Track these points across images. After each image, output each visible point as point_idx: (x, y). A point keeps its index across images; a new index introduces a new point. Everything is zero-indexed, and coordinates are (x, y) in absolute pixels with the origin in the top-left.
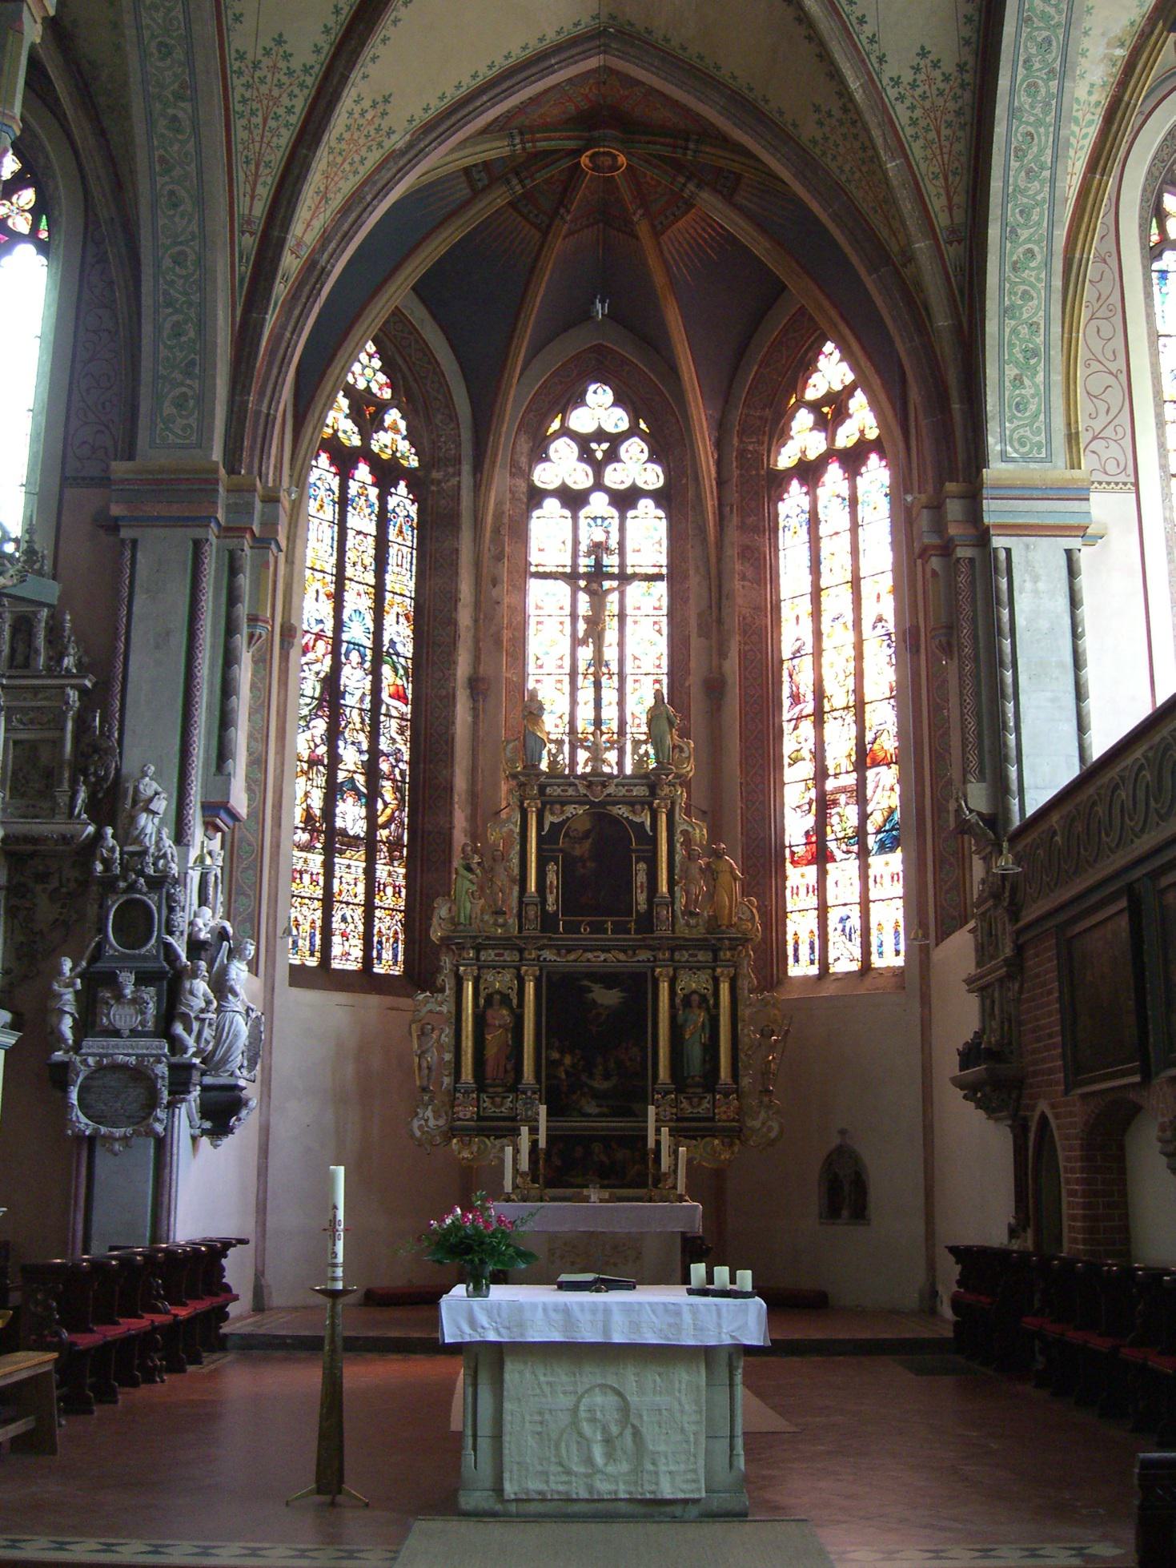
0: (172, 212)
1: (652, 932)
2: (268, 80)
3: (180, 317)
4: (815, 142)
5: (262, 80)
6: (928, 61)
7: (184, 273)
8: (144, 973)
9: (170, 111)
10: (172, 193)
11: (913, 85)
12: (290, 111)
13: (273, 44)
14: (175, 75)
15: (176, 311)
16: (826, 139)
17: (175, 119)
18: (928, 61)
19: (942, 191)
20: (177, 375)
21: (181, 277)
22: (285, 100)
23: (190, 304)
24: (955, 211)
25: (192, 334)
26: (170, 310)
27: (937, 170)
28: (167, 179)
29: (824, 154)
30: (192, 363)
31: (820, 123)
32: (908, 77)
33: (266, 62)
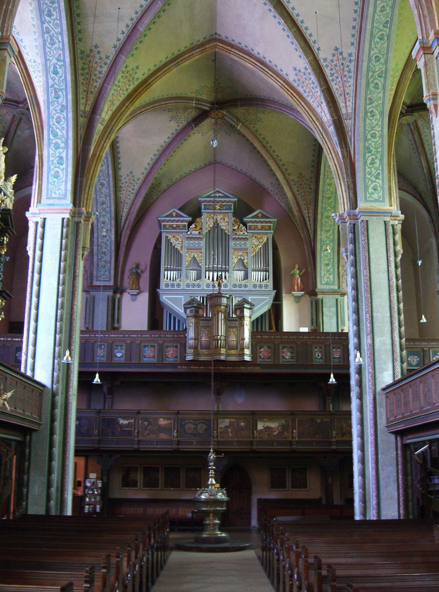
0: (371, 118)
1: (344, 336)
2: (338, 65)
3: (374, 157)
4: (295, 81)
5: (336, 66)
6: (338, 52)
7: (375, 140)
8: (154, 487)
9: (375, 81)
10: (372, 112)
11: (332, 61)
12: (100, 73)
13: (334, 51)
14: (380, 68)
15: (372, 155)
16: (299, 80)
17: (377, 84)
18: (338, 52)
19: (85, 97)
20: (374, 179)
21: (374, 142)
22: (98, 69)
23: (377, 152)
24: (87, 106)
25: (378, 163)
26: (370, 154)
27: (85, 89)
28: (371, 106)
29: (298, 85)
30: (379, 174)
31: (296, 75)
32: (330, 57)
33: (335, 58)
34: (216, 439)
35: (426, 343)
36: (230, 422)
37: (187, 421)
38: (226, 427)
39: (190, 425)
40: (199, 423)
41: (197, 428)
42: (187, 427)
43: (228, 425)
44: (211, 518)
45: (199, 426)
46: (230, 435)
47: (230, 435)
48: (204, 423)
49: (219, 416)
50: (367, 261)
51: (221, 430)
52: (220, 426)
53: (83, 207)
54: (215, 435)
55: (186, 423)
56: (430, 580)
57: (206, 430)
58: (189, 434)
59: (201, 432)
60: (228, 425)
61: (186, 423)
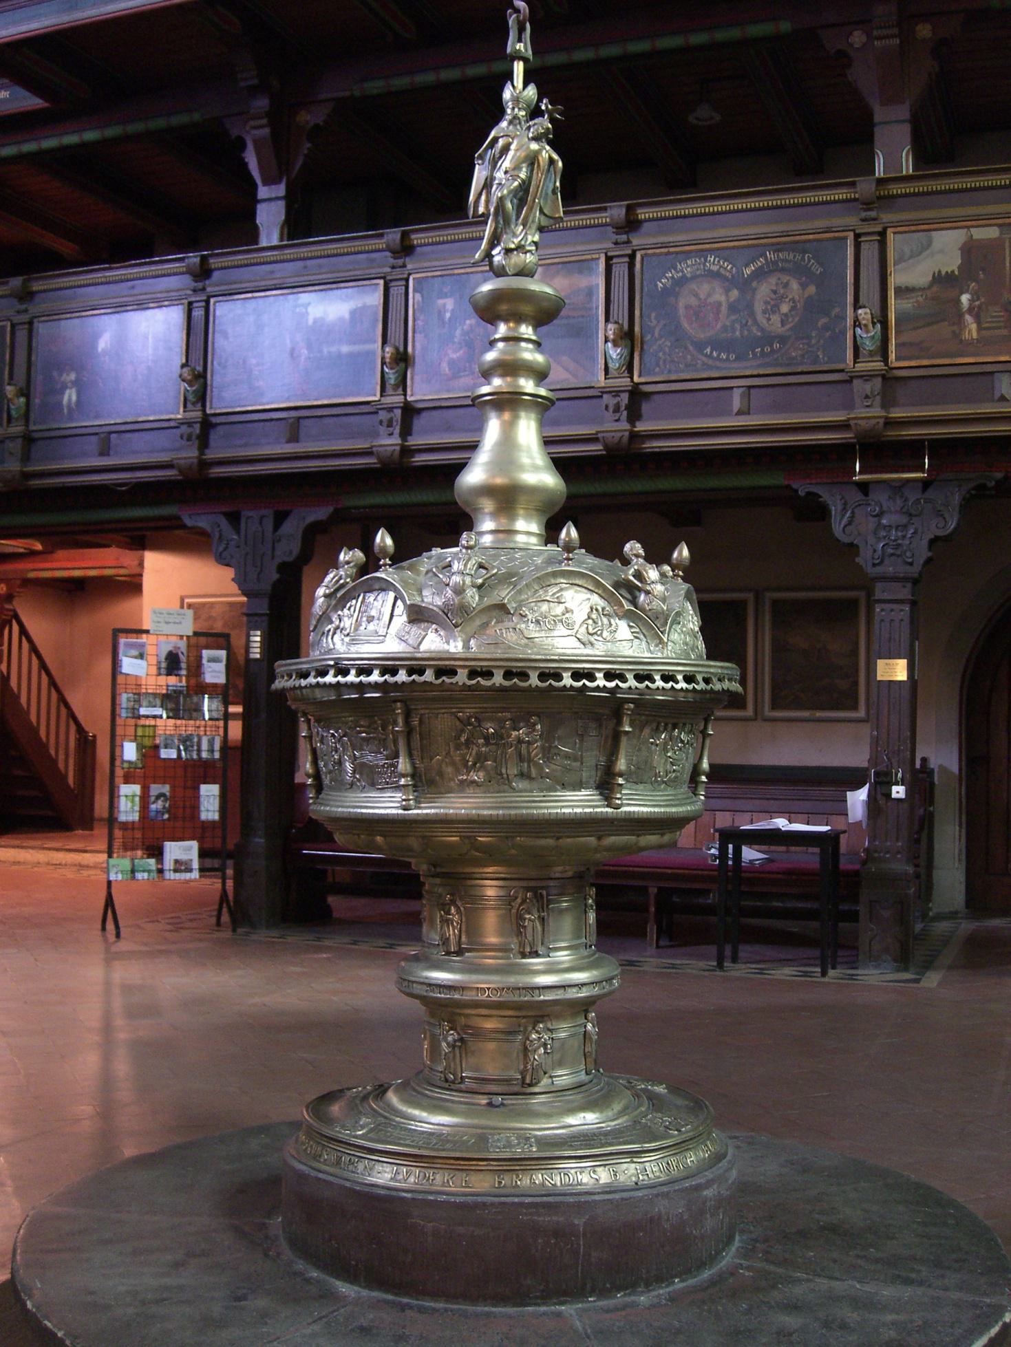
34: (879, 365)
35: (782, 848)
36: (969, 250)
37: (688, 267)
38: (940, 279)
39: (704, 288)
40: (759, 274)
41: (750, 307)
42: (685, 301)
43: (952, 263)
44: (492, 929)
45: (764, 290)
46: (971, 328)
47: (971, 328)
48: (800, 271)
49: (886, 217)
50: (894, 606)
51: (907, 305)
52: (896, 279)
53: (673, 845)
54: (869, 337)
55: (681, 282)
56: (990, 991)
57: (813, 308)
58: (700, 346)
59: (775, 325)
60: (952, 263)
61: (681, 282)
